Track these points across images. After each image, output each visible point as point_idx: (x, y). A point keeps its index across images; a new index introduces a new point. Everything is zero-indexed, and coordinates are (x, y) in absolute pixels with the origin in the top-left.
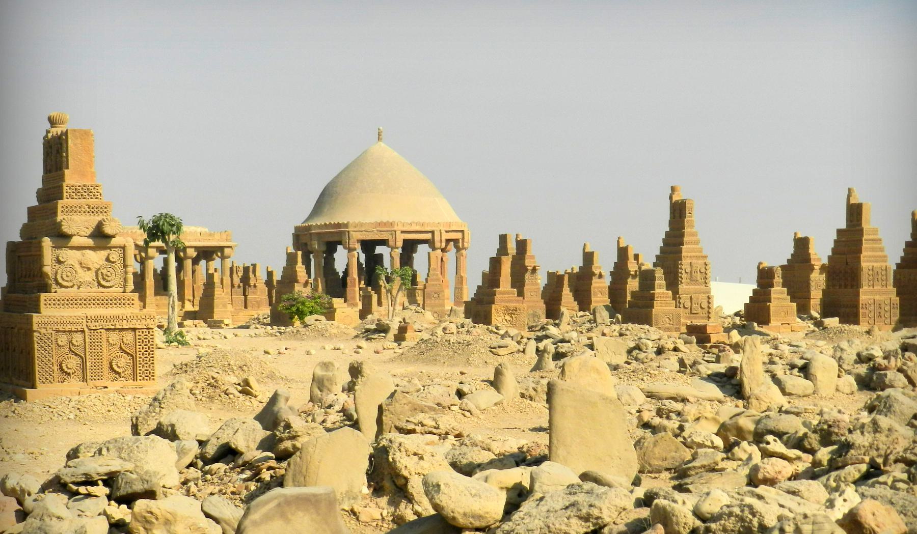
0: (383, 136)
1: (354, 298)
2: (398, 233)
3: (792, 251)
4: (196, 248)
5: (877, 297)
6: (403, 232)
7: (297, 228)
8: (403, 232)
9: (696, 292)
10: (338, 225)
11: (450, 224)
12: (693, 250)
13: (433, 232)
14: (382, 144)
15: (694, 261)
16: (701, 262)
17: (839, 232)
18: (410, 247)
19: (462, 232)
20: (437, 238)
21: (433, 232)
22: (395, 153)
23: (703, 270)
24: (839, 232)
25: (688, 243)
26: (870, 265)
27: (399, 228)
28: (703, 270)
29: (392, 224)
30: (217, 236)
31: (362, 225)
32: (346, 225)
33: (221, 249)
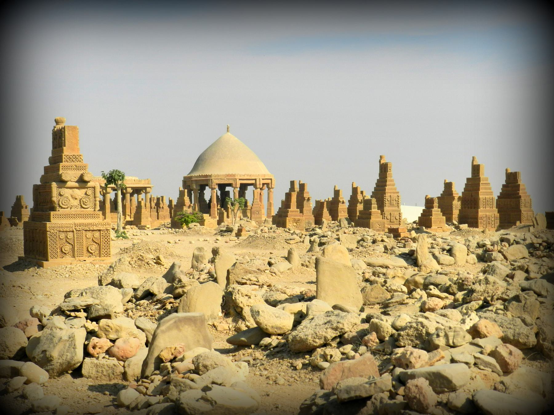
0: (230, 129)
1: (214, 214)
2: (238, 180)
3: (205, 192)
4: (132, 188)
5: (487, 214)
6: (240, 179)
7: (184, 178)
8: (240, 179)
9: (393, 211)
10: (206, 176)
11: (264, 175)
12: (391, 189)
13: (256, 180)
14: (229, 134)
15: (392, 195)
16: (396, 195)
17: (419, 217)
18: (243, 187)
19: (271, 179)
20: (258, 183)
21: (256, 180)
22: (236, 138)
23: (397, 199)
24: (282, 202)
25: (389, 185)
26: (484, 196)
27: (238, 177)
28: (397, 199)
29: (234, 175)
30: (143, 182)
31: (218, 176)
32: (210, 176)
33: (145, 188)
